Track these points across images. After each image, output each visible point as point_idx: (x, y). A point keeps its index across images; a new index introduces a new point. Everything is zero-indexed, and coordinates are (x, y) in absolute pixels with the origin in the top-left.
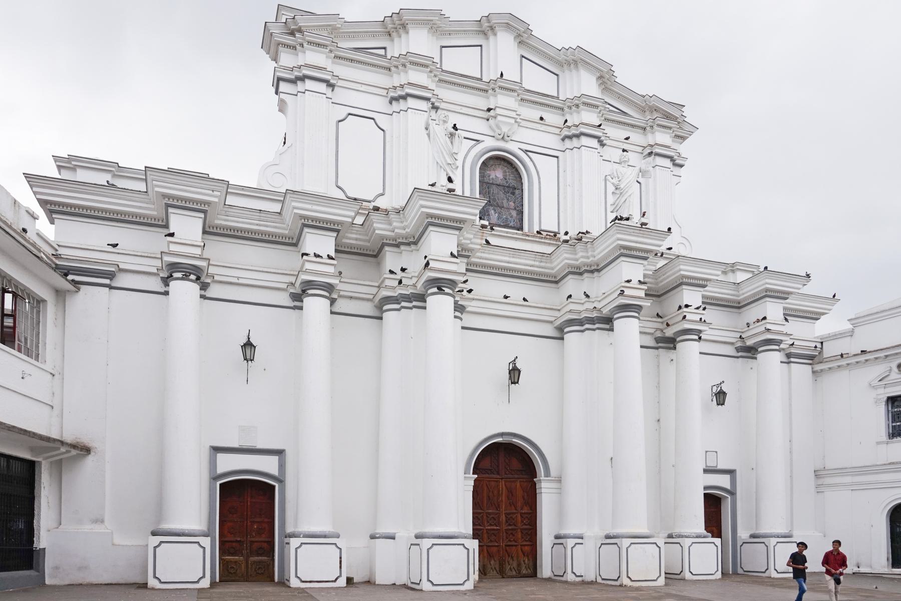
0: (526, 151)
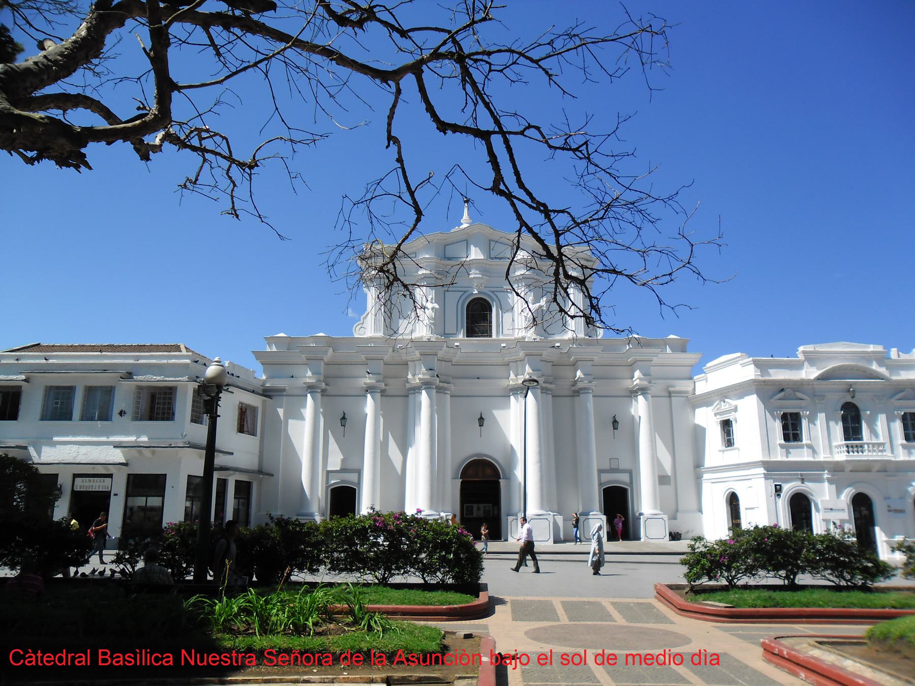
0: (493, 292)
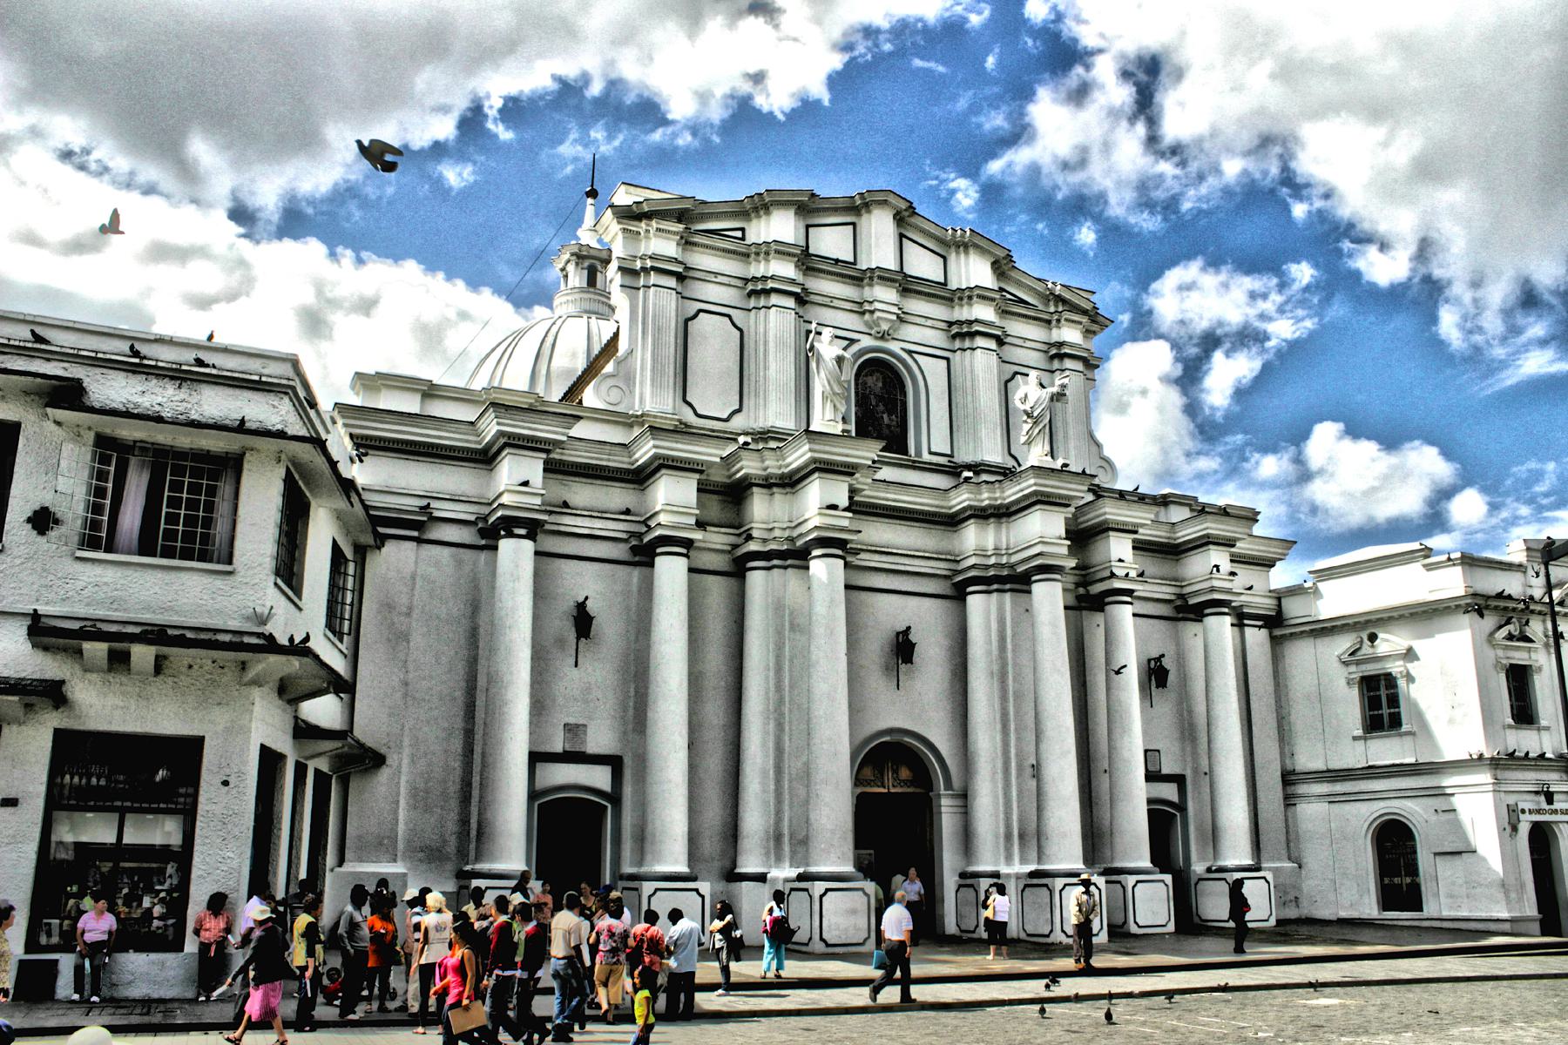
0: (910, 352)
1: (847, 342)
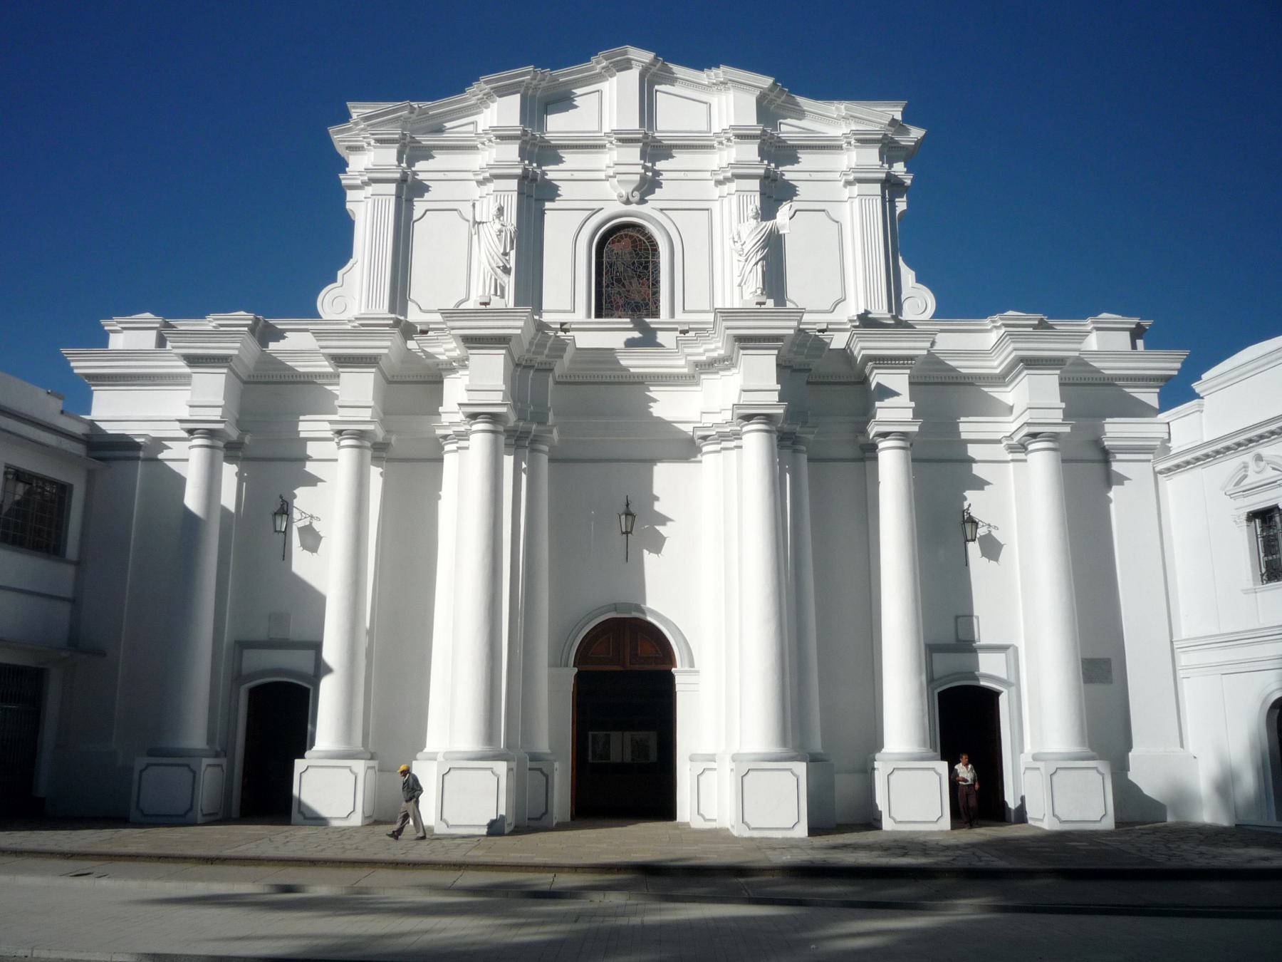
1: (588, 213)
